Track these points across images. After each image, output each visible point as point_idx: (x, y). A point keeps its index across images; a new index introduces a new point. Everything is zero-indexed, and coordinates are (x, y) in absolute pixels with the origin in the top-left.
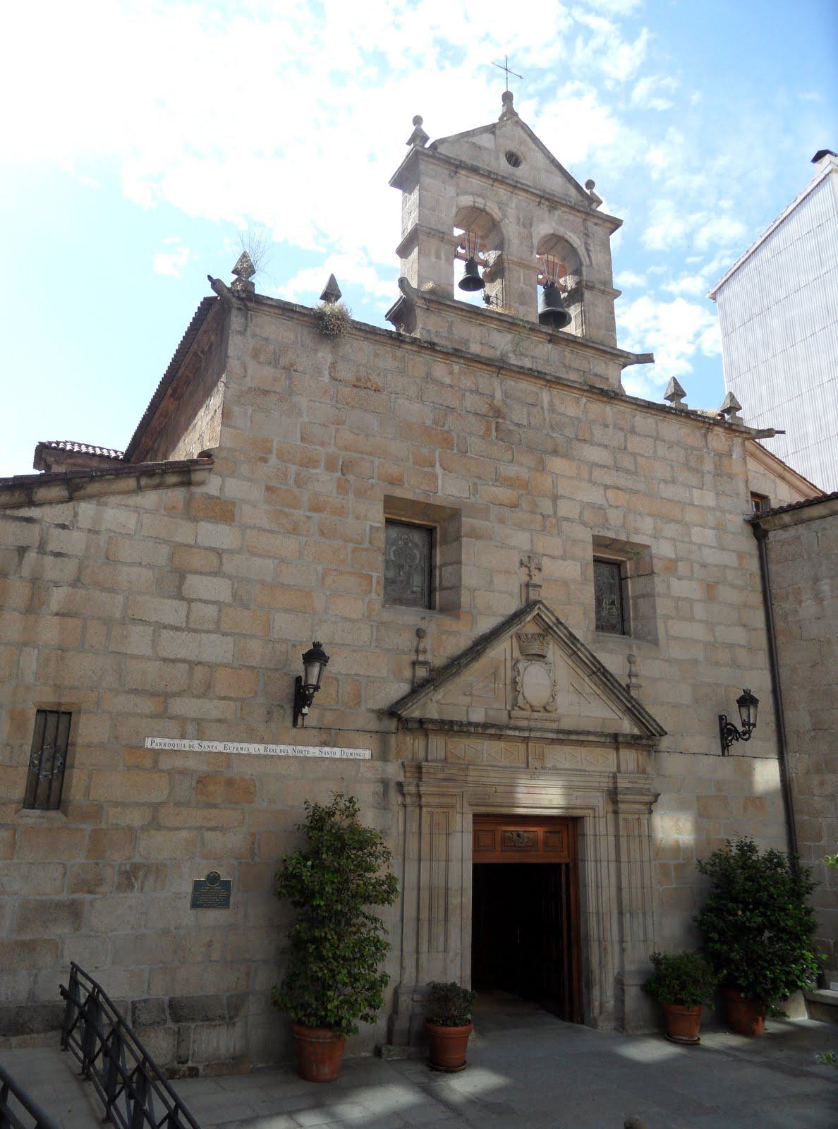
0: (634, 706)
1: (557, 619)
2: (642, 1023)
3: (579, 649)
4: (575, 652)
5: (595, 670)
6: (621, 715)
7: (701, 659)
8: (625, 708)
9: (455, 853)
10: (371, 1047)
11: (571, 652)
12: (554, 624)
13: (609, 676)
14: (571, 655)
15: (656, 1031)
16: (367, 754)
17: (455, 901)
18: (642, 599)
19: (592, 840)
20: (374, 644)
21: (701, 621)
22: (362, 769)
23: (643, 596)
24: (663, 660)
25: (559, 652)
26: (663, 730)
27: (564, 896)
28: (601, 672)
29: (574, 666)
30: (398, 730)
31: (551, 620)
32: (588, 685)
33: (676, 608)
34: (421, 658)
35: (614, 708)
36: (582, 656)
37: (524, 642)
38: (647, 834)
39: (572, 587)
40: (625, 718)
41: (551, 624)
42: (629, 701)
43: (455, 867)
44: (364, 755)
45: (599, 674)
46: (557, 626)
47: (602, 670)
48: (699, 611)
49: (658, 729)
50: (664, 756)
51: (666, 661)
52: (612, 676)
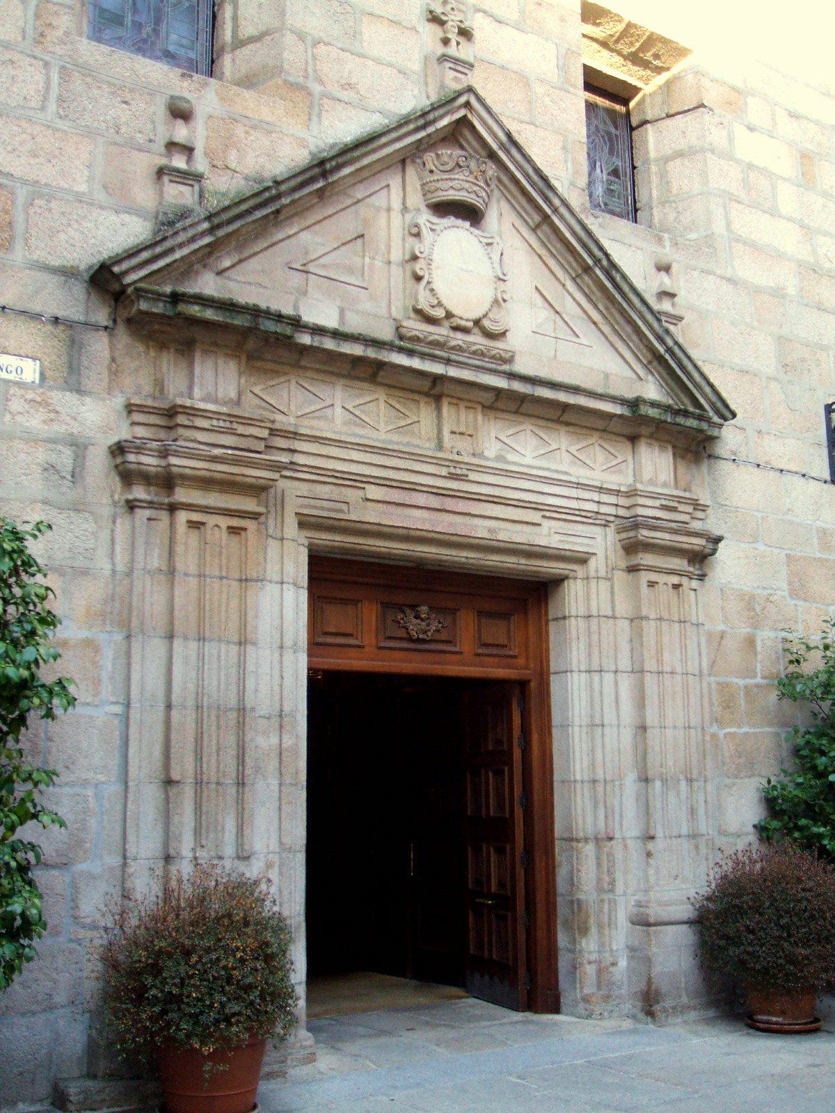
0: (669, 350)
1: (509, 136)
2: (685, 1000)
3: (555, 210)
4: (546, 218)
5: (590, 262)
6: (641, 372)
7: (791, 291)
8: (649, 356)
9: (264, 627)
10: (43, 1089)
11: (537, 218)
12: (502, 146)
13: (618, 278)
14: (538, 226)
15: (711, 1013)
16: (30, 371)
17: (263, 741)
18: (678, 162)
19: (580, 593)
20: (52, 106)
21: (790, 220)
22: (15, 405)
23: (680, 154)
24: (722, 278)
25: (510, 217)
26: (727, 406)
27: (517, 754)
28: (602, 268)
29: (543, 252)
30: (115, 321)
31: (495, 136)
32: (571, 301)
33: (745, 183)
34: (179, 162)
35: (628, 355)
36: (602, 817)
37: (431, 172)
38: (177, 643)
39: (539, 90)
40: (650, 378)
41: (494, 146)
42: (661, 340)
43: (262, 660)
44: (19, 370)
45: (598, 272)
46: (508, 152)
47: (605, 263)
48: (787, 198)
49: (714, 399)
50: (725, 467)
51: (729, 280)
52: (624, 277)
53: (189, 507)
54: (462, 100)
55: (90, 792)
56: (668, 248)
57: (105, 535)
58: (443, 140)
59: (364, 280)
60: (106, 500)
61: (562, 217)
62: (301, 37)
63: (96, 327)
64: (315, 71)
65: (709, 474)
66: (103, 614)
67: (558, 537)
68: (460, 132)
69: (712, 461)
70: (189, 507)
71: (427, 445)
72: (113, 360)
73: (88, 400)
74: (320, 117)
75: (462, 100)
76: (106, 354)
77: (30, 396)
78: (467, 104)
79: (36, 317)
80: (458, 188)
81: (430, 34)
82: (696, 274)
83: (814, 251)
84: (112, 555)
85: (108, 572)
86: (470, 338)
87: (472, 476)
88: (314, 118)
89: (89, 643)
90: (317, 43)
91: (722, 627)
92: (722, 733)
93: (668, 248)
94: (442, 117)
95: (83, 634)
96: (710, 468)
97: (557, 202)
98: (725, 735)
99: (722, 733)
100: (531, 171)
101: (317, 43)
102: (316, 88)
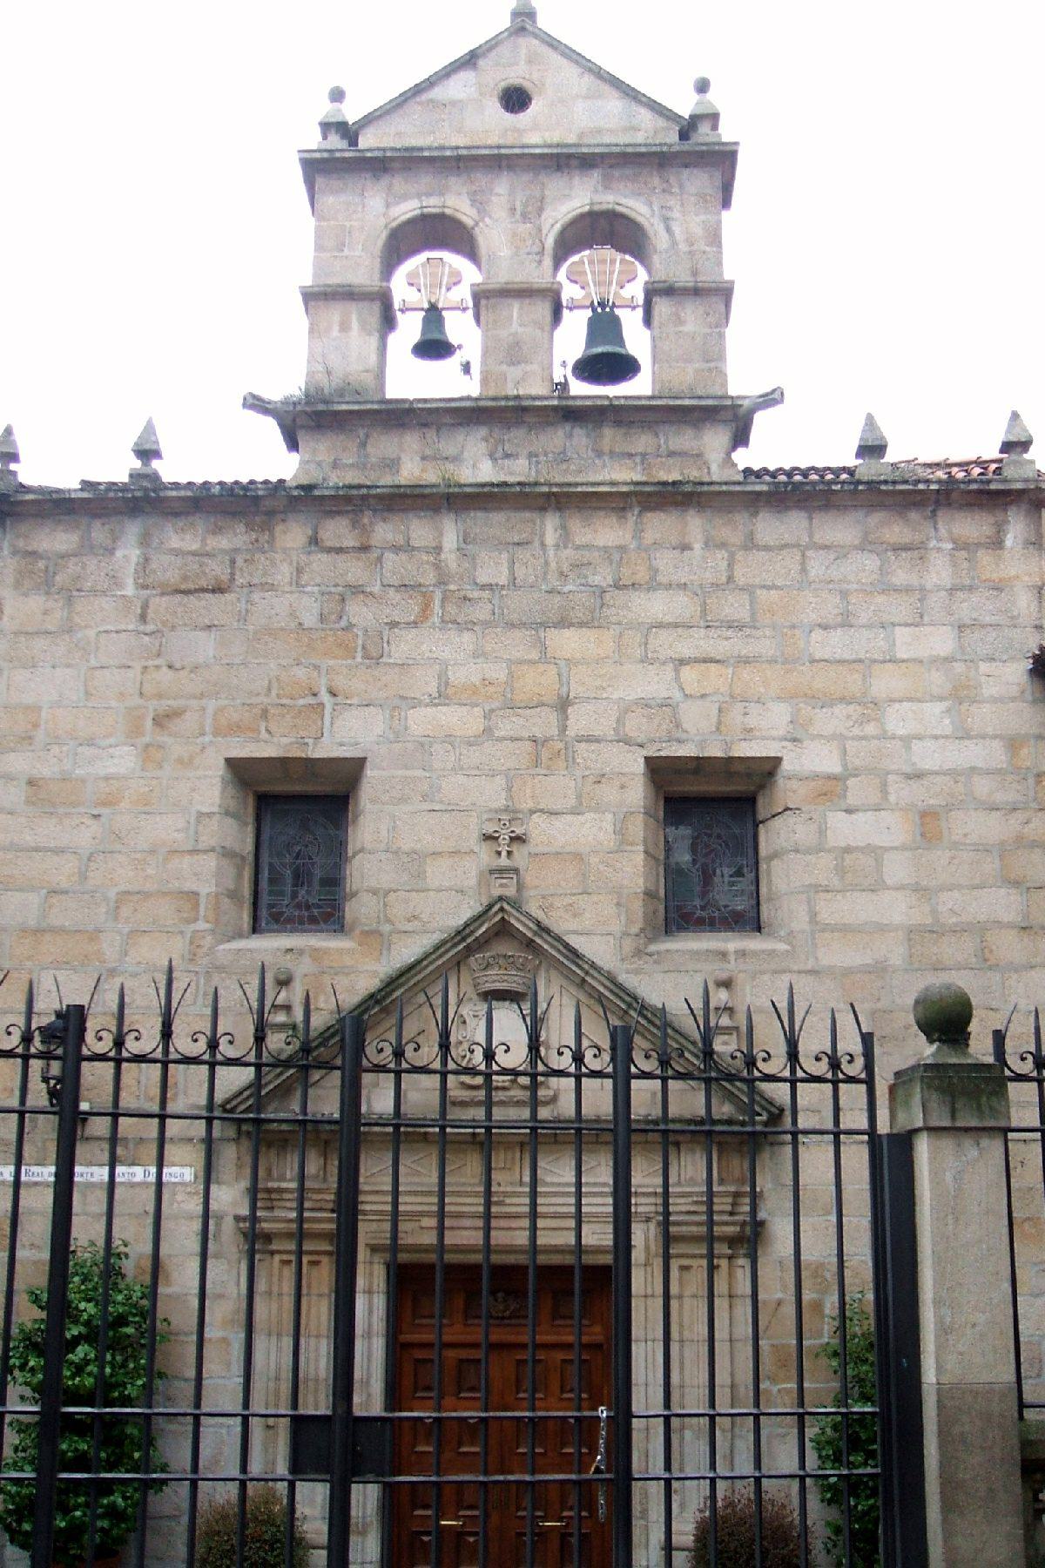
1: (538, 924)
12: (535, 933)
53: (279, 1252)
54: (496, 908)
55: (224, 1431)
56: (733, 962)
57: (234, 1272)
58: (497, 934)
59: (731, 876)
60: (235, 1250)
61: (593, 977)
62: (375, 892)
63: (229, 1140)
64: (386, 916)
65: (771, 1159)
66: (232, 1321)
67: (596, 1236)
68: (503, 930)
69: (776, 1148)
70: (279, 1252)
71: (472, 1181)
72: (239, 1158)
73: (224, 1187)
74: (389, 949)
75: (496, 908)
76: (235, 1155)
77: (189, 1190)
78: (502, 909)
79: (191, 1140)
80: (496, 979)
81: (485, 856)
82: (766, 977)
83: (934, 912)
84: (238, 1284)
85: (235, 1295)
86: (512, 1093)
87: (508, 1201)
88: (385, 952)
89: (224, 1340)
90: (387, 893)
91: (779, 1295)
92: (775, 1389)
93: (733, 962)
94: (481, 925)
95: (220, 1334)
96: (773, 1153)
97: (586, 966)
98: (779, 1391)
99: (775, 1389)
100: (561, 948)
101: (387, 893)
102: (386, 928)
